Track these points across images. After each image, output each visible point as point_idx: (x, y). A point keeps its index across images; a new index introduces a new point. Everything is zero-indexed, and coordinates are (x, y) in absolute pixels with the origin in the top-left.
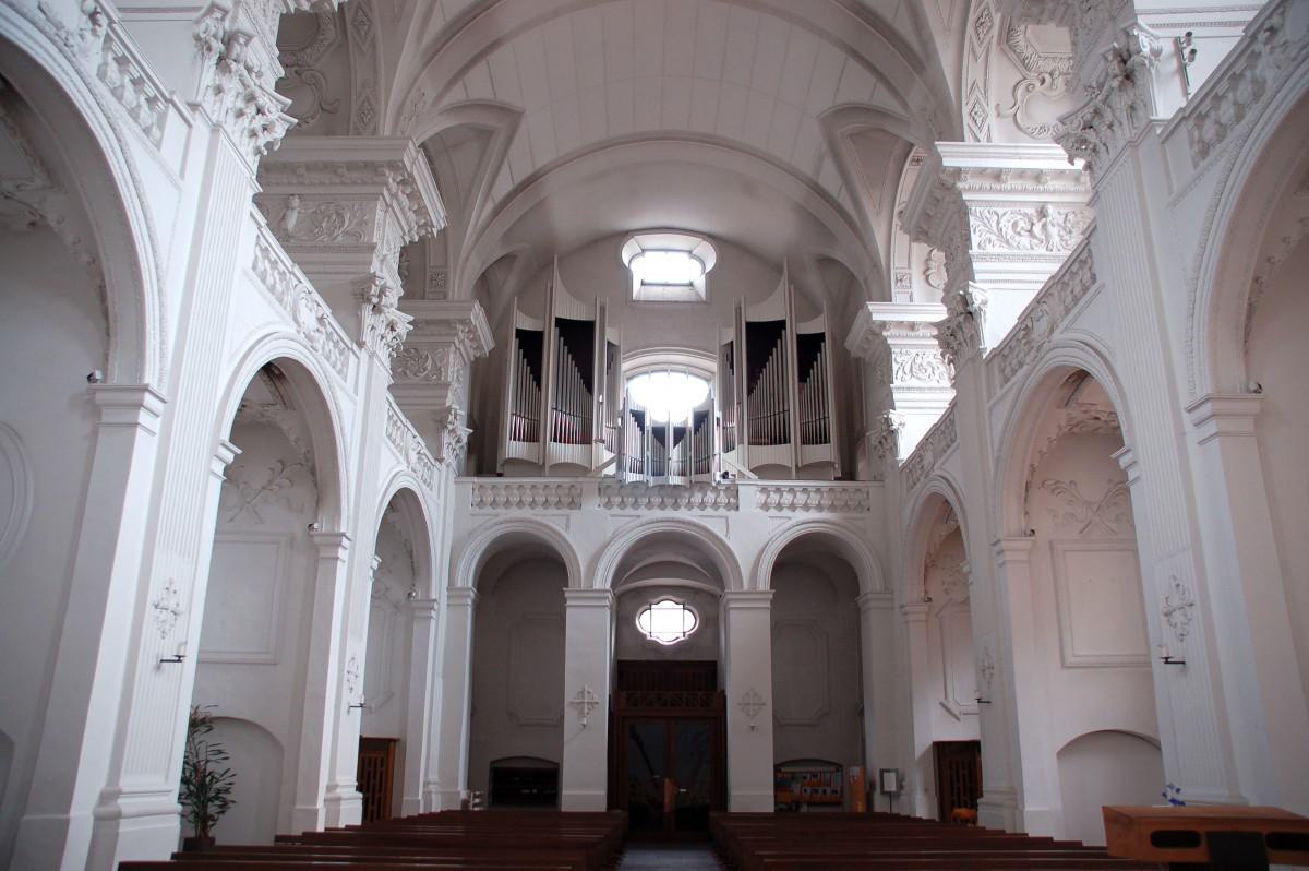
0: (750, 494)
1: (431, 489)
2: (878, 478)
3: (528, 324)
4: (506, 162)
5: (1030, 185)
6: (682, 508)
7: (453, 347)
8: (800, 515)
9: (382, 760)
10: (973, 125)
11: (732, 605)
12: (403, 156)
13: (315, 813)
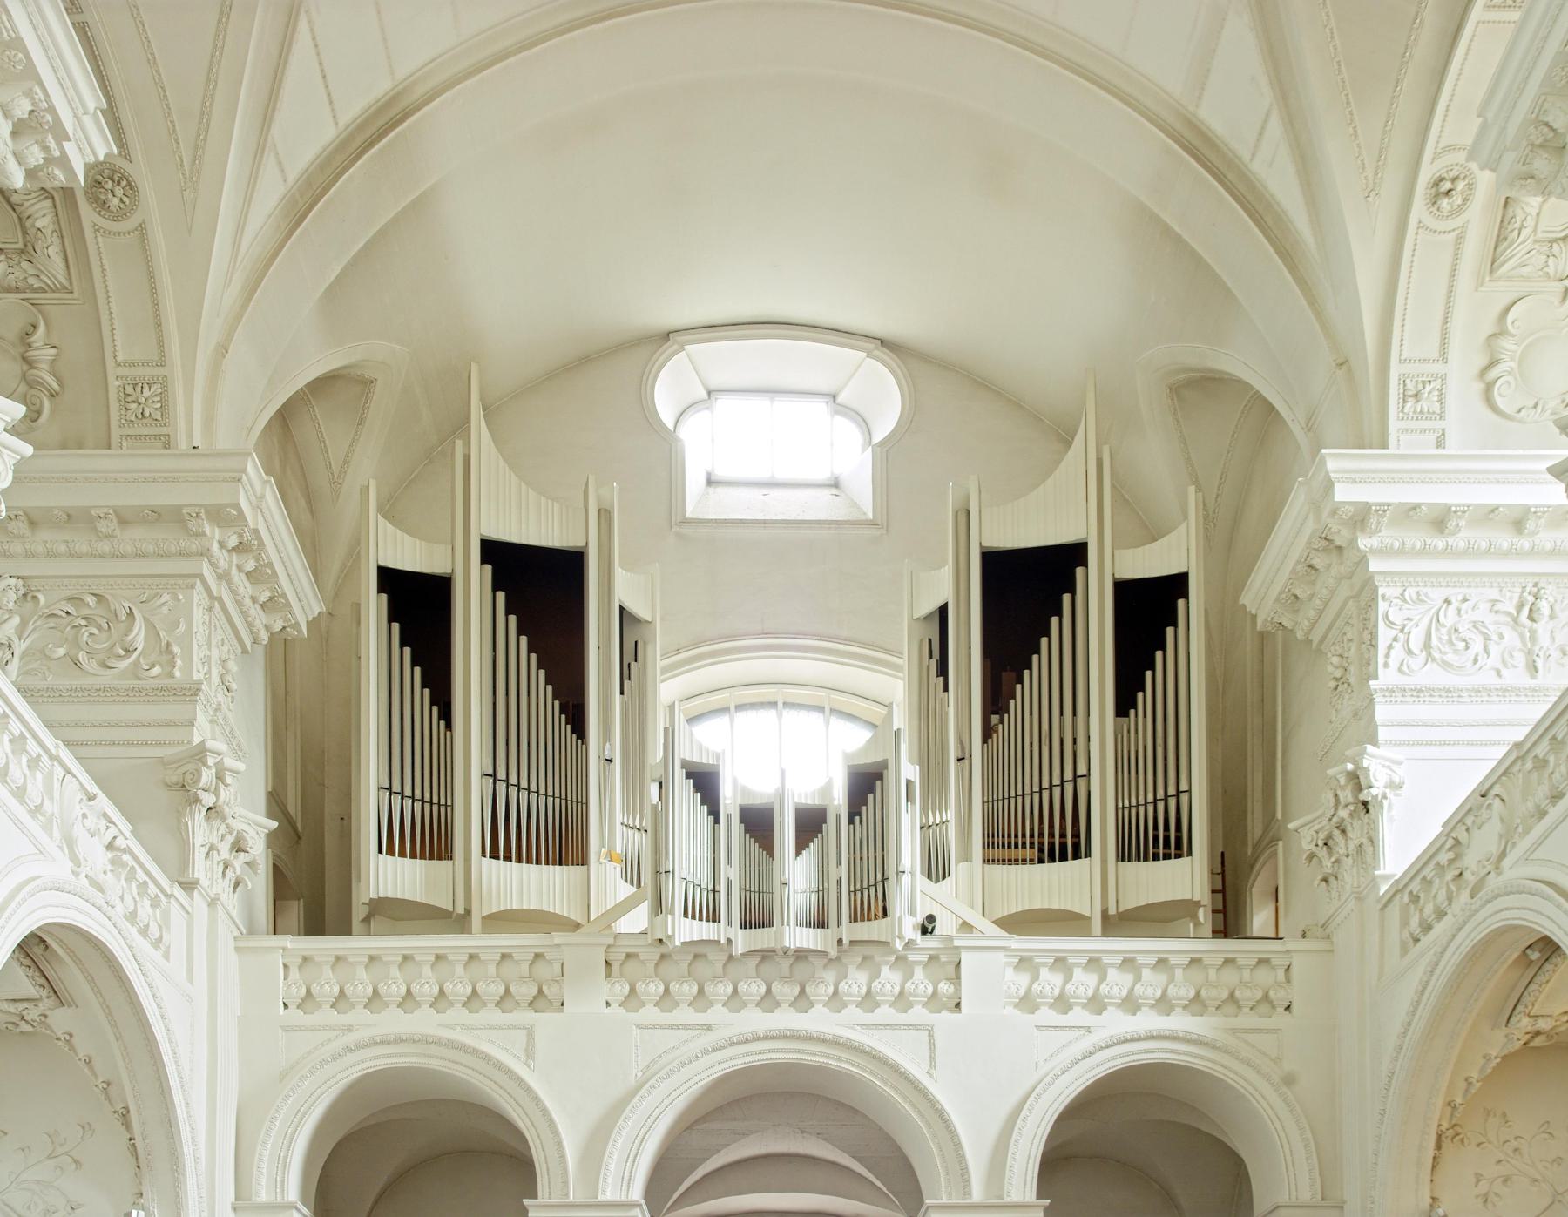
1: (167, 956)
3: (413, 557)
4: (303, 26)
5: (1505, 540)
6: (819, 1008)
7: (199, 596)
8: (1117, 1023)
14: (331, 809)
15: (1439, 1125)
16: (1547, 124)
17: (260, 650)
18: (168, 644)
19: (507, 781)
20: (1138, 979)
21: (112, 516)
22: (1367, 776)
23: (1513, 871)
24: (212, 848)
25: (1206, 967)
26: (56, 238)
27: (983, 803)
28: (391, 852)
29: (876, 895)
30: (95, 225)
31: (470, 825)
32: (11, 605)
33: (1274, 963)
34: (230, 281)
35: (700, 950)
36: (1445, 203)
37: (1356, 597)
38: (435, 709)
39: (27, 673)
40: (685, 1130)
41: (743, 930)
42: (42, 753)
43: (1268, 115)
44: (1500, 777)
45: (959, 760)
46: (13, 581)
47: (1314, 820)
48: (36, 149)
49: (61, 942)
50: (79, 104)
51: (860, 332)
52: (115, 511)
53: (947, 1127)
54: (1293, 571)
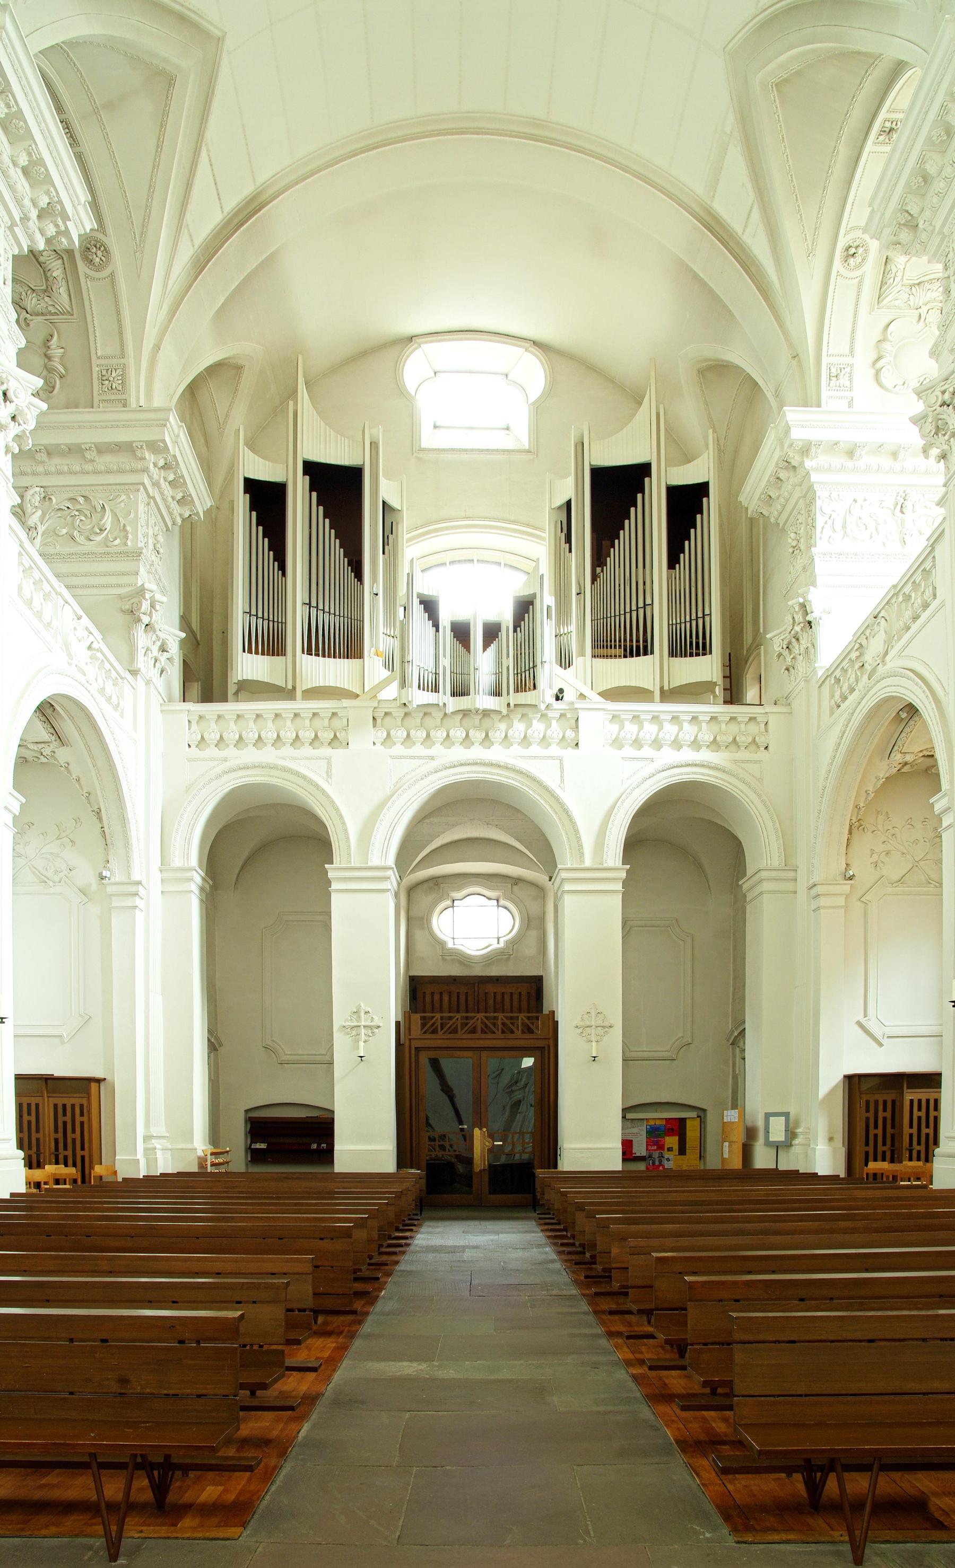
3: (265, 472)
4: (204, 153)
7: (142, 495)
8: (669, 756)
9: (82, 1106)
11: (567, 887)
14: (217, 626)
15: (851, 820)
16: (907, 212)
17: (177, 529)
18: (124, 525)
19: (317, 607)
20: (681, 729)
21: (94, 449)
22: (811, 606)
23: (892, 663)
24: (147, 650)
25: (719, 723)
26: (64, 283)
27: (592, 620)
28: (250, 652)
29: (529, 676)
30: (86, 274)
31: (295, 635)
32: (37, 504)
33: (758, 720)
34: (162, 306)
35: (428, 710)
36: (851, 261)
37: (804, 497)
38: (276, 563)
39: (45, 544)
40: (419, 822)
41: (453, 698)
42: (52, 590)
44: (884, 606)
45: (578, 594)
46: (38, 489)
47: (781, 633)
48: (51, 226)
49: (62, 706)
50: (75, 199)
51: (521, 337)
52: (95, 446)
53: (571, 820)
54: (768, 481)
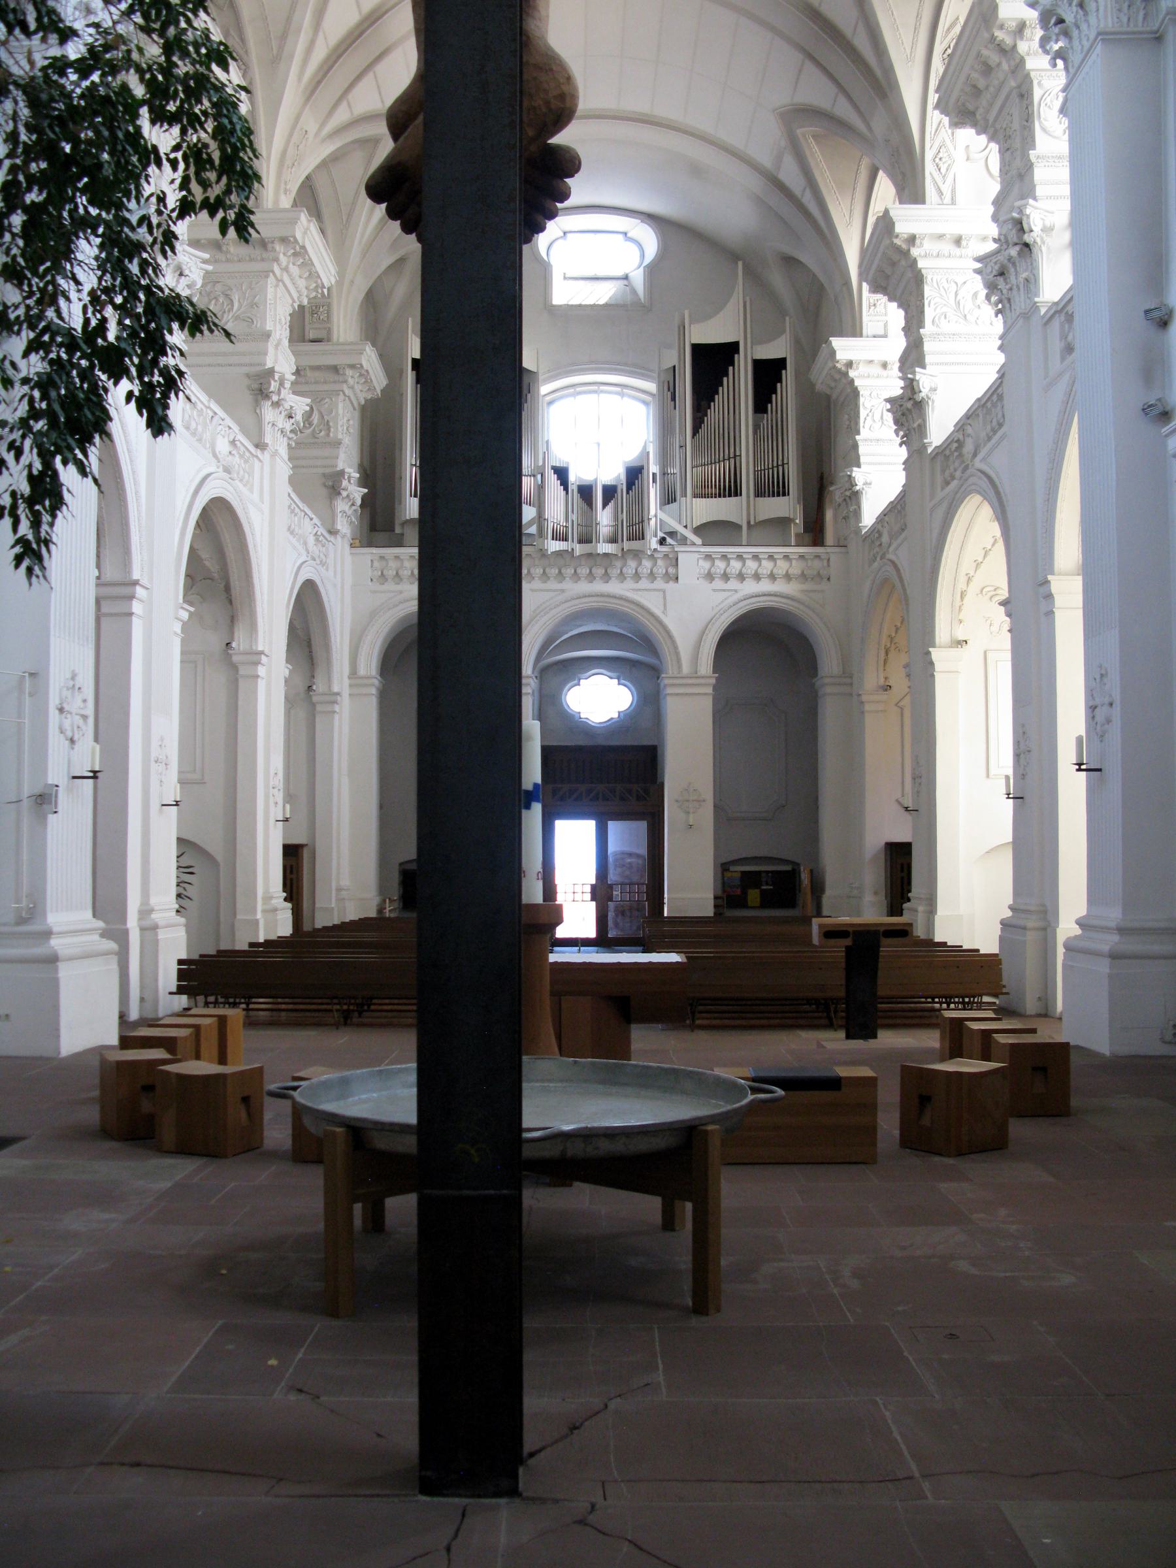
0: (692, 561)
2: (841, 544)
7: (341, 397)
10: (936, 174)
12: (294, 231)
13: (257, 921)
43: (857, 23)
